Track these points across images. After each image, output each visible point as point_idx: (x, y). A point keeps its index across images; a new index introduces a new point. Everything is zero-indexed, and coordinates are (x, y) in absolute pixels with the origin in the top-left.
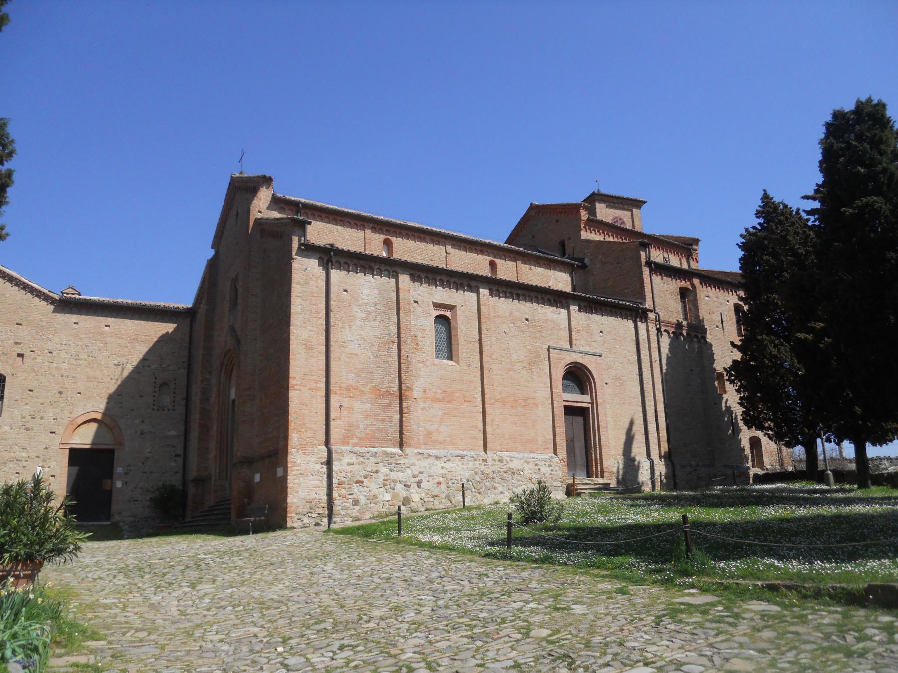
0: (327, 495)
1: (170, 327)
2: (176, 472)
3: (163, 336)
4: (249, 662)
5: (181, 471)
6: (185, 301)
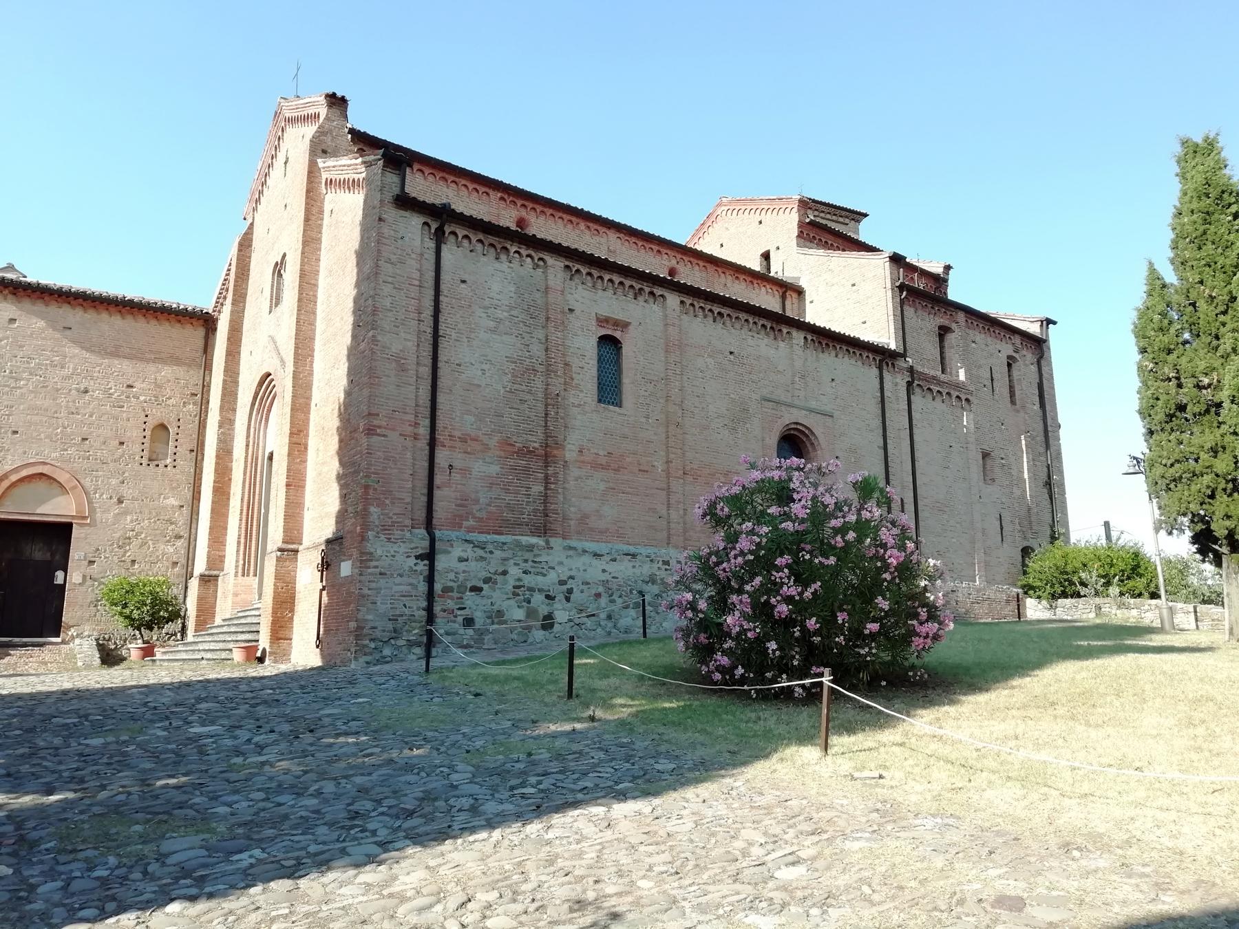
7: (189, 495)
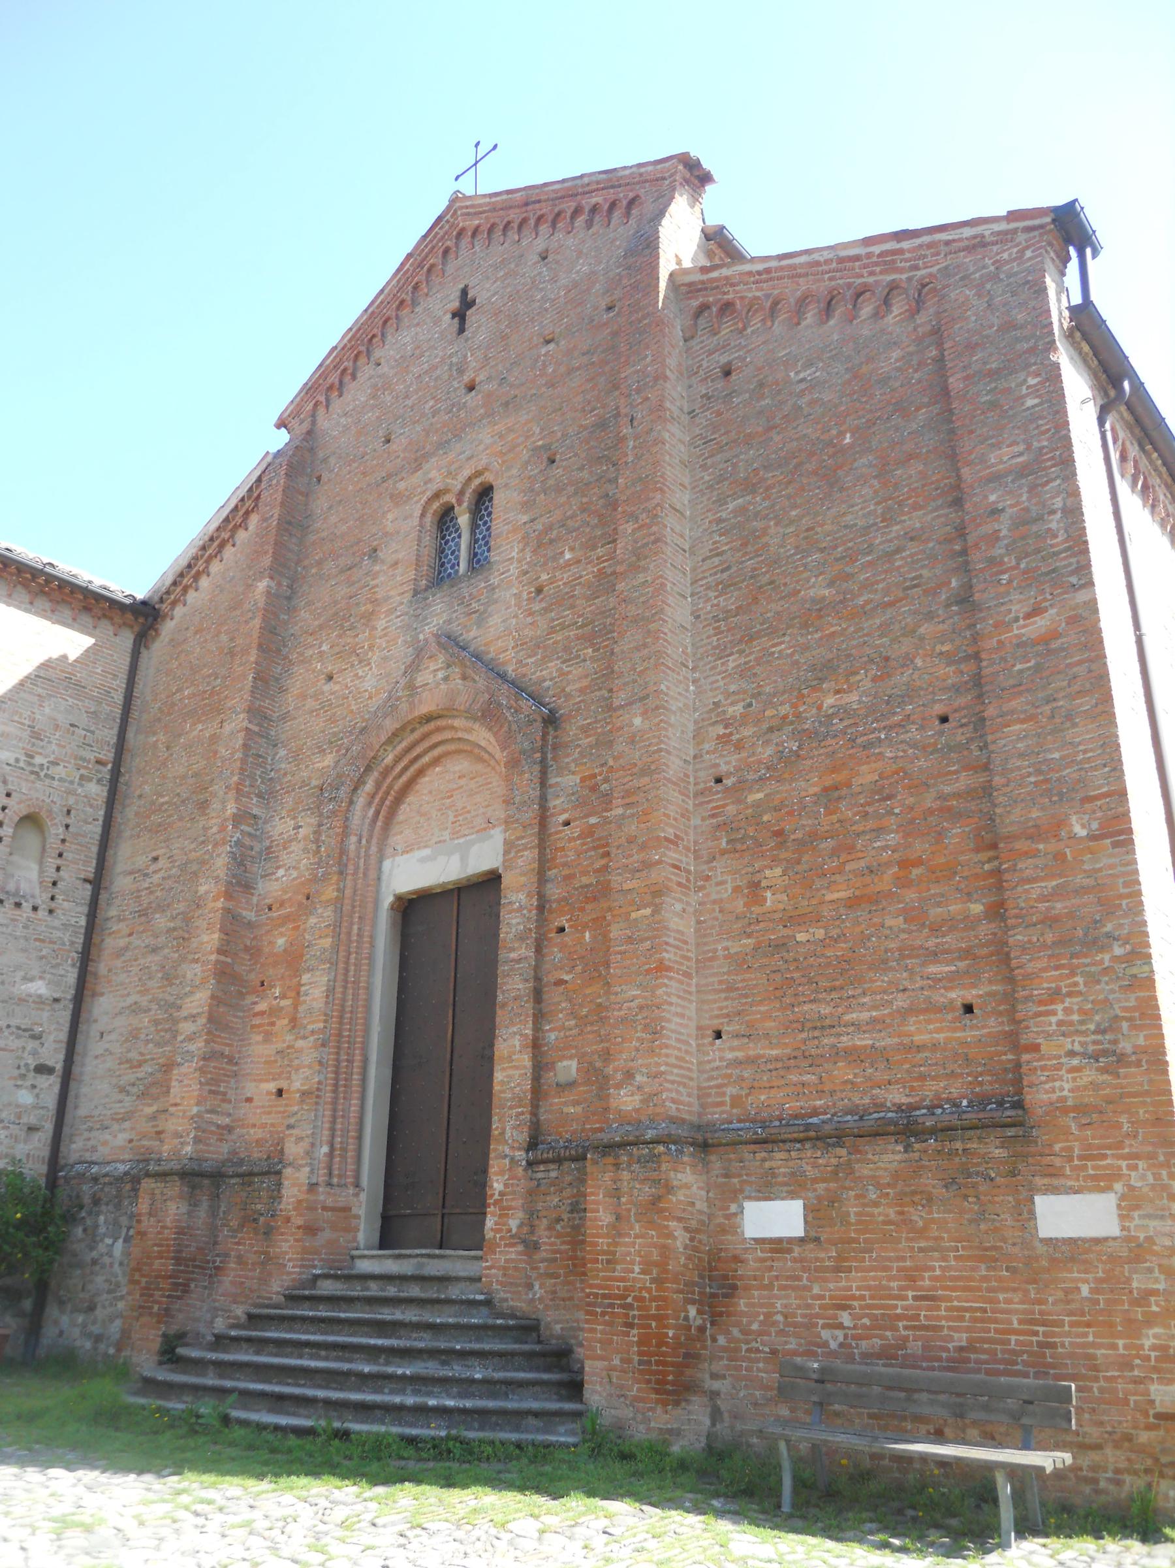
0: (90, 905)
1: (69, 642)
2: (31, 1129)
3: (46, 665)
4: (102, 1180)
5: (49, 1126)
6: (134, 580)
7: (72, 977)
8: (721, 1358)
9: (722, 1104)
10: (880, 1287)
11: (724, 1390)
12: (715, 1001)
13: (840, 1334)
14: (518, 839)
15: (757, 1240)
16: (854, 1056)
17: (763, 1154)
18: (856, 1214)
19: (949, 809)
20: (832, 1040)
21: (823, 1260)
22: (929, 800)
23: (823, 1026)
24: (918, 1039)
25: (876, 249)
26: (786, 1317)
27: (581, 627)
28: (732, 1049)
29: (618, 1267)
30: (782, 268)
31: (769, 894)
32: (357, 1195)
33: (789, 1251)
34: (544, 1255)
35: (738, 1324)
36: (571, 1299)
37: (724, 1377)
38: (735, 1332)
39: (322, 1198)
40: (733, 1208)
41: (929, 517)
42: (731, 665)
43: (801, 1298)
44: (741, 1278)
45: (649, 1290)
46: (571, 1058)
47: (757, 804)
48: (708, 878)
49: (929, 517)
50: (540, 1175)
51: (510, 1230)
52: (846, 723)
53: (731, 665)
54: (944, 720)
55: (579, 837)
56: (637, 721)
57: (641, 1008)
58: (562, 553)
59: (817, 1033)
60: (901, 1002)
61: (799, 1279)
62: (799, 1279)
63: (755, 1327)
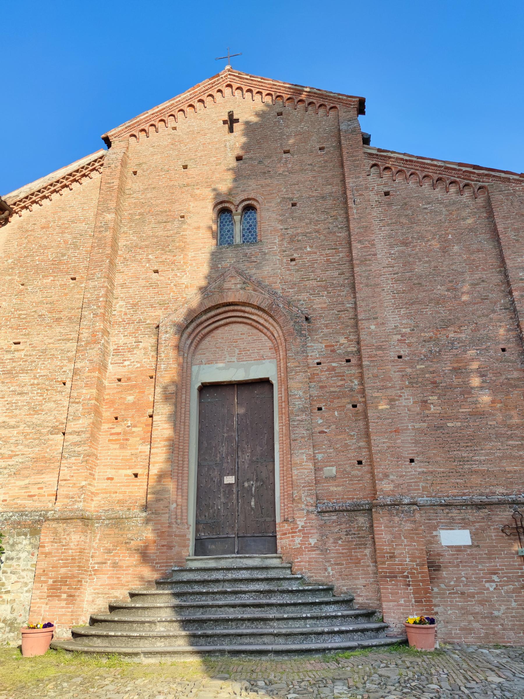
8: (437, 597)
9: (419, 489)
10: (510, 565)
11: (439, 611)
12: (410, 447)
13: (494, 585)
14: (296, 367)
15: (448, 547)
16: (483, 474)
17: (447, 511)
18: (495, 536)
19: (511, 384)
20: (469, 466)
21: (482, 555)
22: (502, 379)
23: (463, 460)
24: (507, 469)
25: (464, 169)
26: (467, 579)
27: (319, 281)
28: (420, 467)
29: (397, 559)
30: (418, 162)
31: (432, 406)
32: (188, 528)
33: (465, 551)
34: (333, 555)
35: (443, 583)
36: (351, 575)
37: (439, 606)
38: (443, 586)
39: (174, 530)
40: (435, 533)
41: (489, 275)
42: (402, 312)
43: (473, 570)
44: (442, 563)
45: (417, 569)
46: (332, 466)
47: (422, 370)
48: (401, 396)
49: (489, 275)
50: (325, 518)
51: (311, 544)
52: (461, 344)
53: (402, 312)
54: (503, 350)
55: (327, 371)
56: (373, 327)
57: (389, 447)
58: (306, 247)
59: (461, 463)
60: (498, 454)
61: (472, 562)
62: (472, 562)
63: (452, 583)
